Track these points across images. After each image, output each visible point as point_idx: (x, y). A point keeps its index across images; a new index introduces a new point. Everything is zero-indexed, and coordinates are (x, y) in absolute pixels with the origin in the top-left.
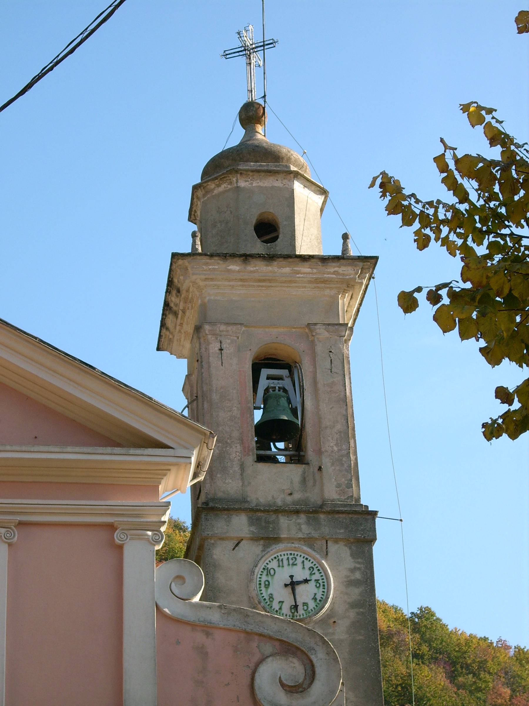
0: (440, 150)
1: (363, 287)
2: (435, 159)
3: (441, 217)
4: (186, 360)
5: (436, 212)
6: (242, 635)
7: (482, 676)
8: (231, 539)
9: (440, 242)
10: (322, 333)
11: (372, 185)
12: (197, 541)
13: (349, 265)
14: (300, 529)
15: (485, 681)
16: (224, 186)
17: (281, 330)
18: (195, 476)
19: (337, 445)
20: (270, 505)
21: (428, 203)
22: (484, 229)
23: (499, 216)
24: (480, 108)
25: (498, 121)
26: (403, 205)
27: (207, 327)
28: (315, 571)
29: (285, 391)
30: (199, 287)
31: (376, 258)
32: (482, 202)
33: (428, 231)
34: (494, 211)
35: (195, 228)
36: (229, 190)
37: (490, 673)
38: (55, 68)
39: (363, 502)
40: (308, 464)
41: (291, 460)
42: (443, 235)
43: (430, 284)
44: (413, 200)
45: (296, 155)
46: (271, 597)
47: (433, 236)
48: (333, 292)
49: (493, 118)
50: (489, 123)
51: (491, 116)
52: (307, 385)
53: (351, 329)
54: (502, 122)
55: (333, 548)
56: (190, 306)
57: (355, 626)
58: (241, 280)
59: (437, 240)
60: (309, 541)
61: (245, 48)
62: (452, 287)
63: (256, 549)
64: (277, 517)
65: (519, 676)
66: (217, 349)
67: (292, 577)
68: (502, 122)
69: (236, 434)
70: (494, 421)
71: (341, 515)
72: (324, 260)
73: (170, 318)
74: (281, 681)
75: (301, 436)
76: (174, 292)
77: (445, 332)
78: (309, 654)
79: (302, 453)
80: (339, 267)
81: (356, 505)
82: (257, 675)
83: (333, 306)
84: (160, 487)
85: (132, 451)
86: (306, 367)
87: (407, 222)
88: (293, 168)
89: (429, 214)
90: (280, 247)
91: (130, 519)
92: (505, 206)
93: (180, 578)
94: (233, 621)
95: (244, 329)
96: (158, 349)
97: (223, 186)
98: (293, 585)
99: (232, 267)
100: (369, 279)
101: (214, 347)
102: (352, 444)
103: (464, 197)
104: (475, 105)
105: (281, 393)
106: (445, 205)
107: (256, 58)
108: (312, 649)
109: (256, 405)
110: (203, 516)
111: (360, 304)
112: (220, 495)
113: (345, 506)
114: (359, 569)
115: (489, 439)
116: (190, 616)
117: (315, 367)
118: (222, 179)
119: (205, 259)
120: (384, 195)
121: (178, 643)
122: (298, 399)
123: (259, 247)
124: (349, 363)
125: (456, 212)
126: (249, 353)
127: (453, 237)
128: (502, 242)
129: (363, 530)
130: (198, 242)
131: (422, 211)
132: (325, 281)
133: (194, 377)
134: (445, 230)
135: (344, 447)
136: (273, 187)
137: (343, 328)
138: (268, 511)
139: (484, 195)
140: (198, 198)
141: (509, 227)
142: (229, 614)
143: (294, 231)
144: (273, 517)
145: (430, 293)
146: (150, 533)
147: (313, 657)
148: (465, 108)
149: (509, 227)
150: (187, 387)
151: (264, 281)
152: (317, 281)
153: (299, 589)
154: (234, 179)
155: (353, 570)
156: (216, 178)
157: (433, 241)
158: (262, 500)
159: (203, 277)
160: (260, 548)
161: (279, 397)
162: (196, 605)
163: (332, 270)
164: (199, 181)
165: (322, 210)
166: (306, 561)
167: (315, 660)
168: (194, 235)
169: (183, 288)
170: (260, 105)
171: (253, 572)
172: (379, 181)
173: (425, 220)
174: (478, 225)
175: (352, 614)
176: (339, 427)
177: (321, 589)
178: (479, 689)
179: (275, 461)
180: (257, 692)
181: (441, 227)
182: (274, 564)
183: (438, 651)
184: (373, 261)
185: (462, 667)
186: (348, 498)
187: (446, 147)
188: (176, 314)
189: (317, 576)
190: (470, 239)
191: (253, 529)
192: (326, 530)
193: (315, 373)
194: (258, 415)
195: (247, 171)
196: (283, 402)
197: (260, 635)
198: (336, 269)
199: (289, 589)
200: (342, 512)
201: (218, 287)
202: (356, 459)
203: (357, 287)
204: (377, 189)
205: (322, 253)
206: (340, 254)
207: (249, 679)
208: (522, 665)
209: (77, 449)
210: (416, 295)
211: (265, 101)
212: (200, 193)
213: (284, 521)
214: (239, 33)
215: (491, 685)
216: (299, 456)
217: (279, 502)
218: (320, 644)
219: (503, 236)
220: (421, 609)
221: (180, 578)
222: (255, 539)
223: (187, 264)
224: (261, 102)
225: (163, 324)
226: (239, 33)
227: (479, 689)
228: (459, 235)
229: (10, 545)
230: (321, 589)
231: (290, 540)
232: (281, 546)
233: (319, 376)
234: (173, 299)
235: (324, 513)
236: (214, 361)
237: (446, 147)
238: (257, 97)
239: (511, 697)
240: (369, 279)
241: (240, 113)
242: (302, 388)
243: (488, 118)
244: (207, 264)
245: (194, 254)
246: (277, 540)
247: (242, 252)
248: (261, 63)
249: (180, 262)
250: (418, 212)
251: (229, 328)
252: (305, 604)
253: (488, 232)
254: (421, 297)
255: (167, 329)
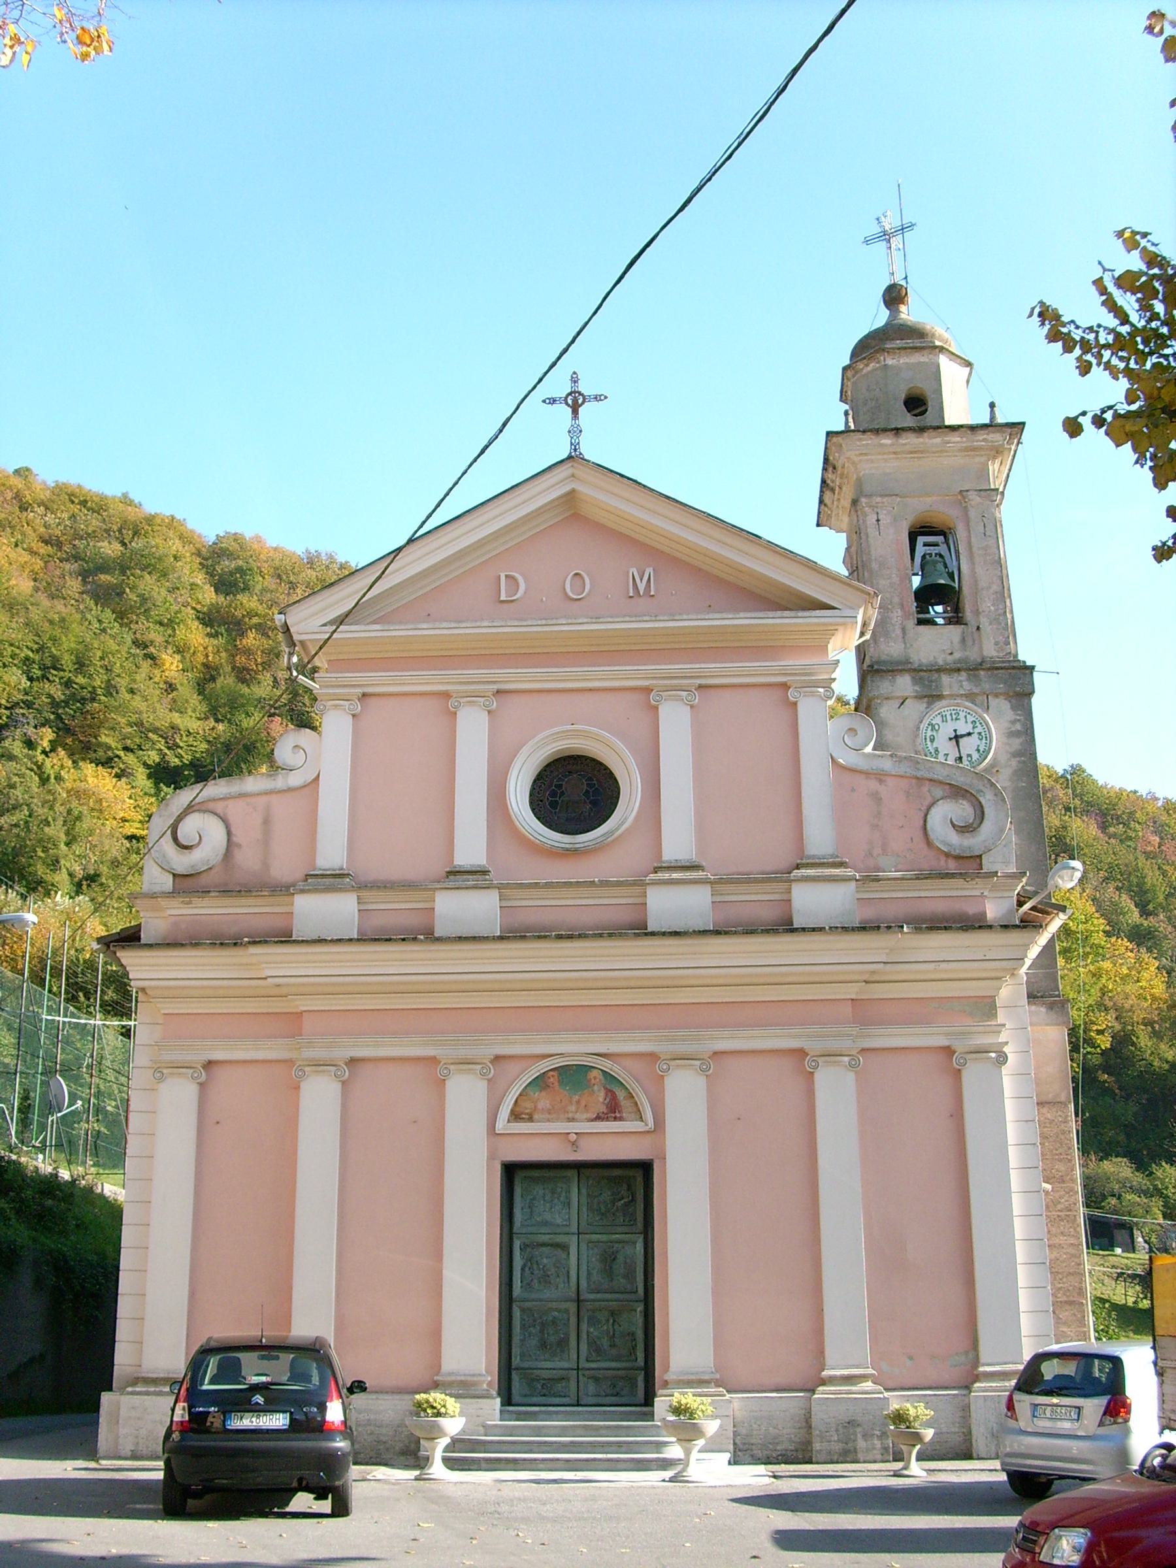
0: (1098, 273)
1: (1012, 453)
2: (1094, 282)
3: (1102, 341)
4: (845, 534)
5: (1097, 338)
6: (914, 781)
7: (1132, 826)
8: (898, 698)
9: (1102, 367)
10: (974, 498)
11: (1031, 315)
12: (864, 702)
13: (998, 431)
14: (962, 686)
15: (1135, 831)
16: (872, 365)
17: (935, 498)
18: (862, 634)
19: (993, 605)
20: (932, 665)
21: (1088, 328)
22: (1147, 350)
23: (1162, 336)
24: (1134, 233)
25: (1153, 244)
26: (1062, 333)
27: (863, 500)
28: (978, 724)
29: (941, 556)
30: (853, 463)
31: (1023, 424)
32: (1143, 323)
33: (1089, 357)
34: (1156, 330)
35: (847, 407)
36: (876, 369)
37: (1139, 823)
38: (713, 178)
39: (1021, 658)
40: (966, 624)
41: (949, 621)
42: (1105, 359)
43: (1095, 408)
44: (1072, 327)
45: (939, 330)
46: (937, 750)
47: (1094, 361)
48: (983, 459)
49: (1148, 241)
50: (1144, 248)
51: (1146, 240)
52: (962, 549)
53: (1003, 493)
54: (1157, 245)
55: (993, 702)
56: (846, 481)
57: (1017, 774)
58: (895, 453)
59: (1099, 364)
60: (971, 697)
61: (885, 233)
62: (1116, 410)
63: (922, 706)
64: (939, 676)
65: (1167, 825)
66: (874, 521)
67: (955, 731)
68: (1157, 245)
69: (896, 600)
70: (1164, 544)
71: (1000, 671)
72: (973, 428)
73: (828, 494)
74: (952, 822)
75: (958, 599)
76: (830, 469)
77: (1117, 446)
78: (978, 796)
79: (960, 615)
80: (988, 434)
81: (1014, 661)
82: (929, 816)
83: (984, 474)
84: (830, 647)
85: (800, 614)
86: (961, 533)
87: (1068, 349)
88: (937, 343)
89: (1089, 340)
90: (929, 418)
91: (803, 678)
92: (1167, 325)
93: (852, 731)
94: (904, 769)
95: (899, 499)
96: (818, 525)
97: (871, 365)
98: (957, 738)
99: (883, 441)
100: (1018, 445)
101: (871, 519)
102: (1008, 603)
103: (1125, 320)
104: (1129, 230)
105: (938, 558)
106: (1105, 328)
107: (896, 242)
108: (980, 791)
109: (915, 572)
110: (869, 678)
111: (1010, 470)
112: (884, 657)
113: (1003, 662)
114: (1019, 720)
115: (1159, 562)
116: (863, 765)
117: (969, 532)
118: (870, 358)
119: (859, 436)
120: (1043, 324)
121: (853, 790)
122: (955, 563)
123: (909, 420)
124: (1001, 525)
125: (1118, 335)
126: (905, 522)
127: (1115, 361)
128: (1165, 363)
129: (1022, 684)
130: (851, 420)
131: (1083, 338)
132: (974, 449)
133: (853, 549)
134: (1107, 354)
135: (1001, 607)
136: (919, 363)
137: (995, 493)
138: (931, 671)
139: (1145, 316)
140: (848, 379)
141: (1172, 346)
142: (900, 762)
143: (942, 402)
144: (936, 675)
145: (1095, 416)
146: (821, 690)
147: (981, 799)
148: (1120, 234)
149: (1172, 346)
150: (847, 559)
151: (915, 452)
152: (967, 449)
153: (962, 741)
154: (882, 358)
155: (1013, 722)
156: (864, 358)
157: (1094, 366)
158: (924, 661)
159: (857, 452)
160: (925, 705)
161: (937, 562)
162: (868, 755)
163: (981, 438)
164: (848, 362)
165: (968, 382)
166: (968, 716)
167: (983, 802)
168: (846, 414)
169: (839, 465)
170: (902, 286)
171: (918, 728)
172: (1037, 310)
173: (1086, 346)
174: (1141, 347)
175: (1014, 763)
176: (995, 587)
177: (984, 741)
178: (1130, 838)
179: (935, 624)
180: (930, 833)
181: (1103, 351)
182: (938, 720)
183: (1089, 803)
184: (1021, 426)
185: (1112, 819)
186: (1007, 654)
187: (1105, 270)
188: (833, 490)
189: (979, 729)
190: (1132, 362)
191: (917, 688)
192: (986, 686)
193: (969, 537)
194: (916, 581)
195: (893, 348)
196: (940, 567)
197: (931, 780)
198: (985, 436)
199: (954, 741)
200: (1002, 668)
201: (872, 461)
202: (1013, 618)
203: (1006, 453)
204: (1036, 319)
205: (970, 422)
206: (987, 421)
207: (922, 822)
208: (1169, 815)
209: (749, 615)
210: (1080, 419)
211: (907, 283)
212: (849, 373)
213: (945, 679)
214: (878, 219)
215: (1140, 834)
216: (958, 617)
217: (941, 662)
218: (988, 786)
219: (1166, 357)
220: (1072, 766)
221: (852, 731)
222: (919, 697)
223: (841, 441)
224: (903, 283)
225: (821, 501)
226: (878, 219)
227: (1130, 838)
228: (1121, 359)
229: (692, 707)
230: (984, 741)
231: (952, 696)
232: (944, 702)
233: (973, 540)
234: (830, 476)
235: (983, 669)
236: (872, 532)
237: (1105, 270)
238: (899, 279)
239: (1160, 845)
240: (1018, 445)
241: (884, 295)
242: (957, 552)
243: (1143, 242)
244: (860, 440)
245: (847, 431)
246: (940, 697)
247: (893, 426)
248: (901, 246)
249: (835, 439)
250: (1078, 338)
251: (885, 500)
252: (969, 755)
253: (1151, 353)
254: (1086, 422)
255: (825, 505)
